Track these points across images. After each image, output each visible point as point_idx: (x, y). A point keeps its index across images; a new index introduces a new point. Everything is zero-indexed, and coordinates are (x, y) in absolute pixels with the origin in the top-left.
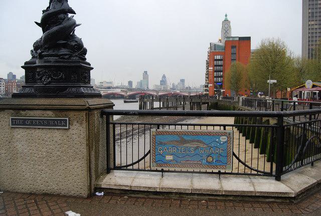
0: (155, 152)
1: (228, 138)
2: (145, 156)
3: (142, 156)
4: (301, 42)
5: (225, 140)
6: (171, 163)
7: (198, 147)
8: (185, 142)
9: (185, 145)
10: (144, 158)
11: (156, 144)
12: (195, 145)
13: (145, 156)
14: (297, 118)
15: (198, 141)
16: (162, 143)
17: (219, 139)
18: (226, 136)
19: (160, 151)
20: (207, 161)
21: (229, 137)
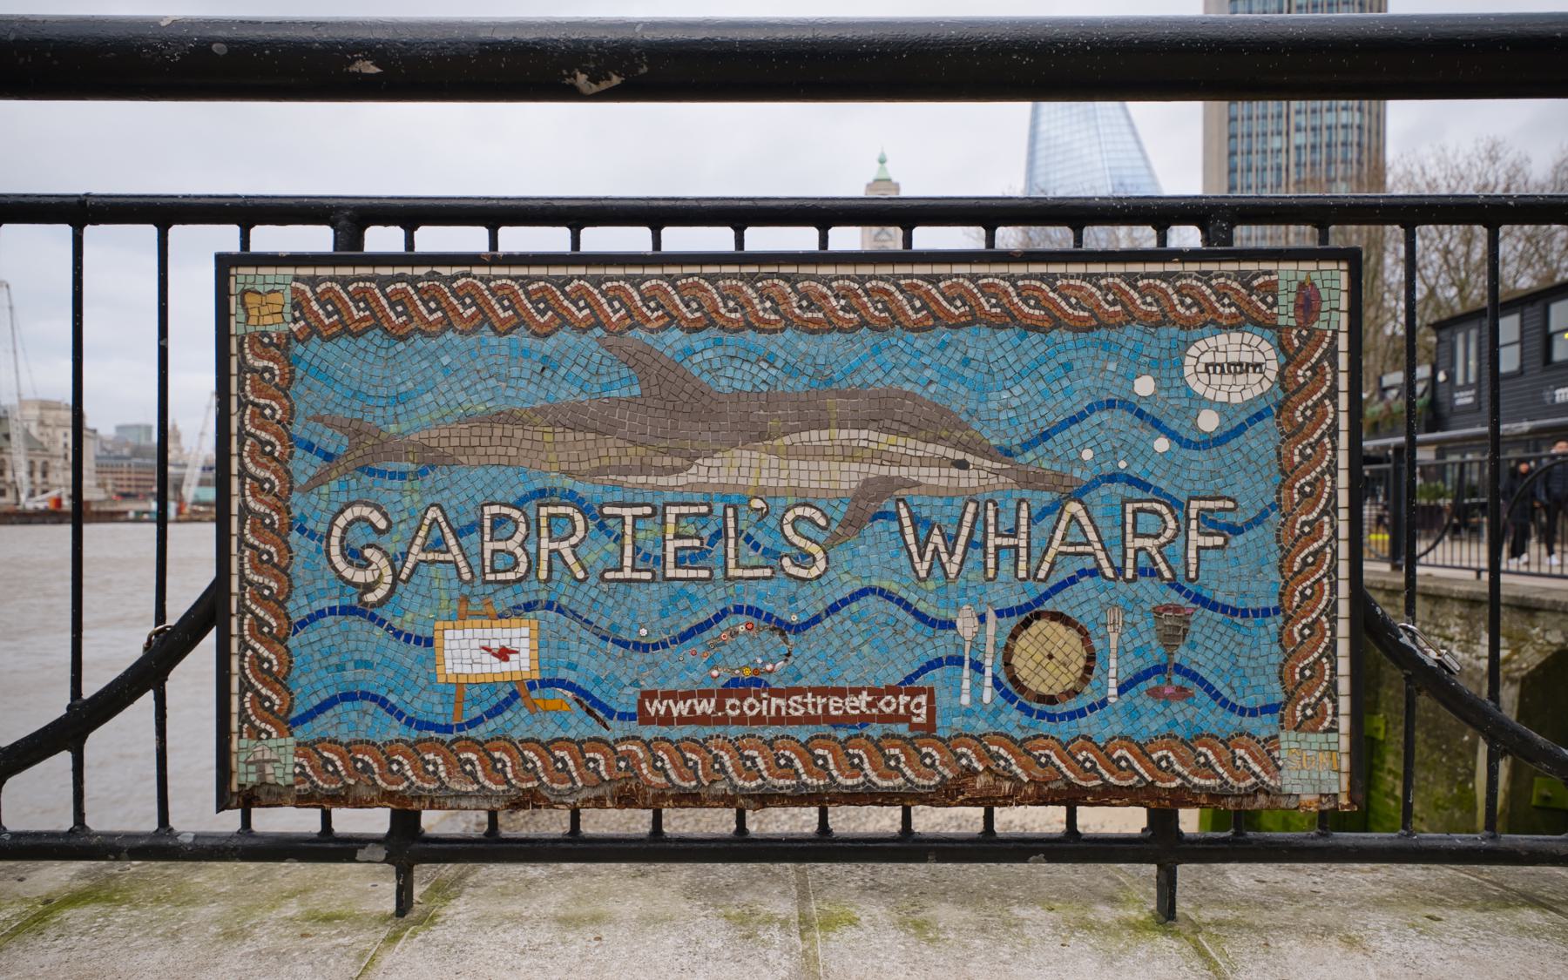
0: (283, 572)
1: (1290, 358)
2: (166, 650)
3: (115, 648)
4: (131, 707)
5: (1249, 389)
6: (518, 723)
7: (889, 485)
8: (684, 413)
9: (698, 474)
10: (149, 674)
11: (304, 466)
12: (826, 469)
13: (166, 650)
14: (1513, 240)
15: (885, 412)
16: (384, 446)
17: (1168, 366)
18: (1265, 324)
19: (355, 556)
20: (1012, 688)
21: (1313, 338)
